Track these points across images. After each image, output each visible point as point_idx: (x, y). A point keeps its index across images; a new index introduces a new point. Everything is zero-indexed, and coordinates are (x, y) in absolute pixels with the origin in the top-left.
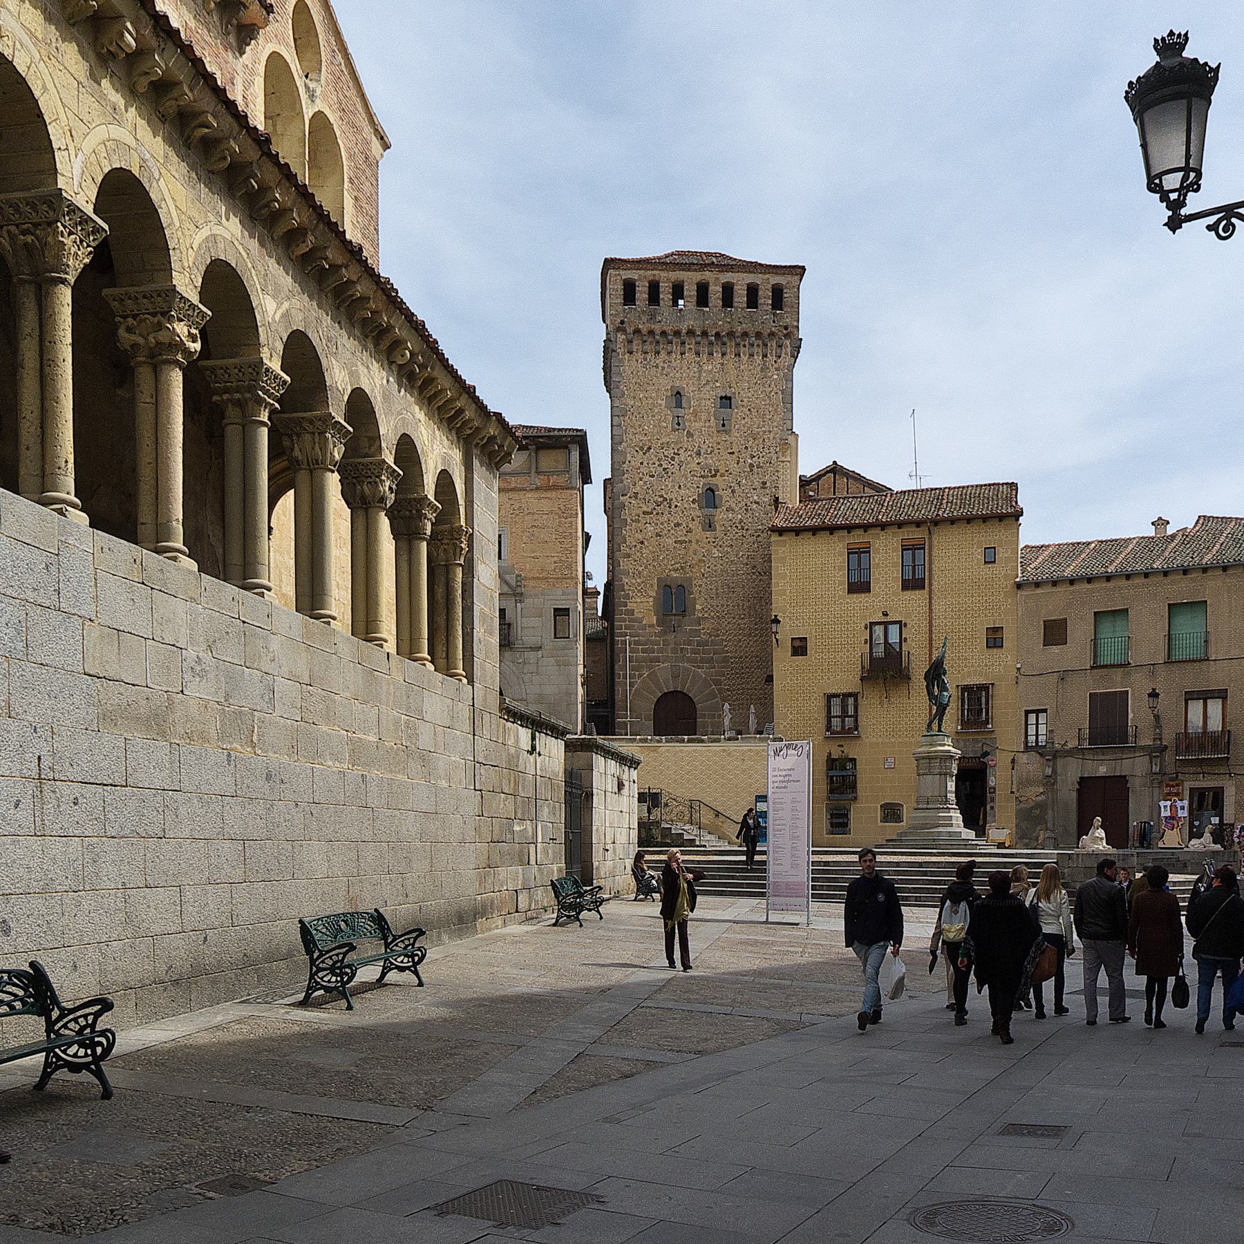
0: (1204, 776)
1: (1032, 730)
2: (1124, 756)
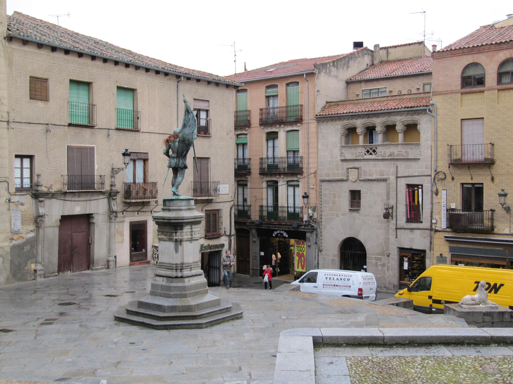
0: (138, 214)
1: (27, 173)
2: (92, 198)
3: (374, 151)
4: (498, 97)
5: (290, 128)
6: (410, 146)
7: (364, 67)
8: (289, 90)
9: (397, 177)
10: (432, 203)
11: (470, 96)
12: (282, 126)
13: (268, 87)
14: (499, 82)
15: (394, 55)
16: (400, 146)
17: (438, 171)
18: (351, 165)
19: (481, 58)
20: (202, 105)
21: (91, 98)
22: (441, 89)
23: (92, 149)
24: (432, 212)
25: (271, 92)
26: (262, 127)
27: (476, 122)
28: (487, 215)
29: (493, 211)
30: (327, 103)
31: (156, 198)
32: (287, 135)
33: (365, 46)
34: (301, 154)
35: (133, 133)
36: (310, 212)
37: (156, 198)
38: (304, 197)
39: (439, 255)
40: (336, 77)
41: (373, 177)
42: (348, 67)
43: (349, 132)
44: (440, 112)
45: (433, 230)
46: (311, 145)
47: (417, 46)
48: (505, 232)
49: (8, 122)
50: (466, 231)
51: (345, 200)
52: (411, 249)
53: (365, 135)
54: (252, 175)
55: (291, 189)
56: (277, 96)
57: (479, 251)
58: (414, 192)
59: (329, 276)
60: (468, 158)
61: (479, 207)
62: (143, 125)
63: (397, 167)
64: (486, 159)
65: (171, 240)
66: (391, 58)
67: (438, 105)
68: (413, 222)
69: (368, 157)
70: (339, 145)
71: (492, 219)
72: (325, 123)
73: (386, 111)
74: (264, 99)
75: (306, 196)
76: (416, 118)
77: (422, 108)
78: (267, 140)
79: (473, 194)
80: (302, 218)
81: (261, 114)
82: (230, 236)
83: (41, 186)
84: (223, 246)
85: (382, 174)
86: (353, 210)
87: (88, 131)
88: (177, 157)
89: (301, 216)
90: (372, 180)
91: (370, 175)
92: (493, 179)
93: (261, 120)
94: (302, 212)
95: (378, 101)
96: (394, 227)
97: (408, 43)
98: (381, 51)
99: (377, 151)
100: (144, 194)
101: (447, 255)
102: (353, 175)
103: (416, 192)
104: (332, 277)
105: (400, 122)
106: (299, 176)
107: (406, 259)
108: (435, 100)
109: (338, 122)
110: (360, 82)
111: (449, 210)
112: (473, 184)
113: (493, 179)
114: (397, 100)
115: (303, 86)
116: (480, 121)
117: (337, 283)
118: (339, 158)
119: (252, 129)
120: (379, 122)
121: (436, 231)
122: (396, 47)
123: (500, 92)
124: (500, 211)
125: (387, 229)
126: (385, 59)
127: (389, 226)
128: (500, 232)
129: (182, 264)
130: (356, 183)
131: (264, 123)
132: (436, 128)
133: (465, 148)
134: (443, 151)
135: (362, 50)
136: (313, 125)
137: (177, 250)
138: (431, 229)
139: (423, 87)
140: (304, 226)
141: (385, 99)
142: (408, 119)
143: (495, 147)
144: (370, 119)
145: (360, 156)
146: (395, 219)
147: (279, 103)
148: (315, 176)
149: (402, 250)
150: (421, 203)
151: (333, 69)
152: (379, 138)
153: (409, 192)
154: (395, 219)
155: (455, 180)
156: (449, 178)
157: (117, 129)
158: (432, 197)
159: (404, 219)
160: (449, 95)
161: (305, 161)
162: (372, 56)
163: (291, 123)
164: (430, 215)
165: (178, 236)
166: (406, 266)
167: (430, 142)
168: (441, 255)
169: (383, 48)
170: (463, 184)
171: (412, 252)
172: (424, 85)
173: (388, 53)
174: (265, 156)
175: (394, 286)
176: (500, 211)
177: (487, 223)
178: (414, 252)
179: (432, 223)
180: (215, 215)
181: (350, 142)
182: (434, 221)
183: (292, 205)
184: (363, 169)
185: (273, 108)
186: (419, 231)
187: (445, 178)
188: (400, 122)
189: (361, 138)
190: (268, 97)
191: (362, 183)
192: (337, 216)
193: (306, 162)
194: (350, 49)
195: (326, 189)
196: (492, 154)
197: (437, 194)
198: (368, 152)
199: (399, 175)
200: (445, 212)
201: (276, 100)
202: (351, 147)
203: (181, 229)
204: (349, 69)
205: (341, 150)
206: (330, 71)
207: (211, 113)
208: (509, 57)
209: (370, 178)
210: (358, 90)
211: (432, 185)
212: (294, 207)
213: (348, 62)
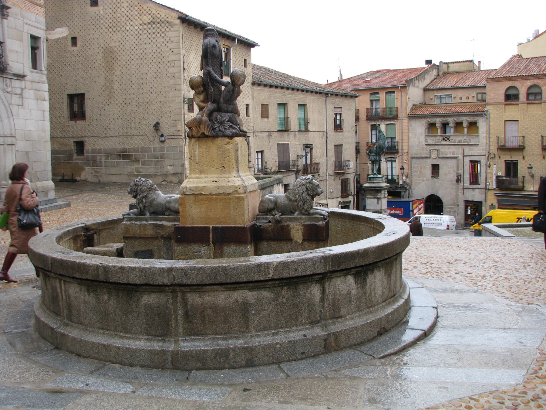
2: (289, 174)
3: (448, 139)
4: (527, 108)
5: (389, 122)
6: (472, 136)
7: (433, 77)
8: (387, 97)
9: (464, 156)
10: (486, 172)
11: (510, 107)
12: (383, 121)
13: (371, 94)
14: (528, 99)
15: (452, 68)
16: (465, 136)
17: (490, 152)
18: (432, 148)
19: (517, 84)
20: (338, 111)
21: (286, 113)
22: (492, 101)
23: (288, 144)
24: (486, 178)
25: (374, 97)
26: (368, 121)
27: (513, 122)
28: (520, 180)
29: (524, 177)
30: (413, 105)
31: (319, 173)
32: (386, 127)
33: (433, 63)
34: (397, 140)
35: (306, 132)
36: (404, 178)
37: (319, 173)
38: (401, 169)
39: (491, 205)
40: (418, 87)
41: (448, 156)
42: (424, 79)
43: (430, 126)
44: (492, 116)
45: (487, 189)
46: (404, 134)
47: (469, 63)
48: (530, 190)
49: (253, 132)
50: (507, 189)
51: (428, 171)
52: (473, 201)
53: (441, 129)
54: (360, 154)
55: (389, 164)
56: (379, 100)
57: (516, 201)
58: (474, 165)
59: (428, 219)
60: (509, 144)
61: (516, 175)
62: (311, 127)
63: (464, 150)
64: (520, 146)
65: (375, 198)
66: (451, 70)
67: (491, 111)
68: (474, 184)
69: (444, 142)
70: (424, 134)
71: (523, 182)
72: (414, 120)
73: (456, 114)
74: (369, 102)
75: (402, 168)
76: (476, 119)
77: (480, 113)
78: (372, 130)
79: (512, 167)
80: (398, 183)
81: (367, 112)
82: (354, 195)
83: (268, 168)
84: (350, 202)
85: (454, 153)
86: (434, 177)
87: (286, 134)
88: (375, 155)
89: (397, 181)
90: (447, 158)
91: (446, 155)
92: (524, 158)
93: (367, 116)
94: (398, 179)
95: (449, 106)
96: (462, 188)
97: (462, 60)
98: (444, 66)
99: (450, 139)
100: (314, 170)
101: (496, 204)
102: (434, 154)
103: (476, 165)
104: (430, 219)
105: (465, 121)
106: (396, 155)
107: (469, 208)
108: (488, 108)
109: (423, 119)
110: (433, 90)
111: (497, 177)
112: (512, 161)
113: (524, 158)
114: (462, 105)
115: (397, 94)
116: (516, 122)
117: (433, 222)
118: (424, 143)
119: (360, 122)
120: (451, 121)
121: (489, 190)
122: (454, 63)
123: (528, 105)
124: (528, 177)
125: (457, 189)
126: (446, 71)
127: (458, 187)
128: (528, 190)
129: (381, 210)
130: (436, 159)
131: (369, 118)
132: (489, 126)
133: (507, 139)
134: (493, 139)
135: (432, 66)
136: (405, 122)
137: (378, 203)
138: (486, 189)
139: (477, 95)
140: (400, 187)
141: (454, 104)
142: (471, 119)
143: (525, 138)
144: (445, 118)
145: (438, 142)
146: (462, 183)
147: (381, 105)
148: (407, 155)
149: (467, 202)
150: (479, 172)
151: (416, 82)
152: (451, 131)
153: (472, 165)
154: (462, 183)
155: (501, 158)
156: (497, 157)
157: (299, 131)
158: (486, 169)
159: (468, 182)
160: (497, 106)
161: (400, 145)
162: (438, 69)
163: (390, 119)
164: (485, 180)
165: (379, 196)
166: (469, 212)
167: (485, 135)
168: (492, 204)
169: (444, 63)
170: (505, 161)
171: (473, 203)
172: (477, 94)
173: (448, 67)
174: (370, 141)
175: (462, 225)
176: (528, 177)
177: (520, 184)
178: (474, 203)
179: (486, 185)
180: (345, 182)
181: (430, 132)
182: (488, 184)
183: (390, 174)
184: (441, 150)
185: (376, 109)
186: (478, 190)
187: (495, 157)
188: (465, 121)
189: (439, 130)
190: (371, 101)
191: (440, 160)
192: (423, 181)
193: (401, 145)
194: (423, 65)
195: (415, 164)
196: (524, 142)
197: (489, 167)
198: (444, 139)
199: (465, 155)
200: (495, 178)
201: (378, 103)
202: (432, 136)
203: (381, 192)
204: (425, 80)
205: (425, 138)
206: (415, 83)
207: (343, 115)
208: (533, 84)
209: (446, 156)
210: (432, 95)
211: (486, 162)
212: (392, 175)
213: (425, 75)
